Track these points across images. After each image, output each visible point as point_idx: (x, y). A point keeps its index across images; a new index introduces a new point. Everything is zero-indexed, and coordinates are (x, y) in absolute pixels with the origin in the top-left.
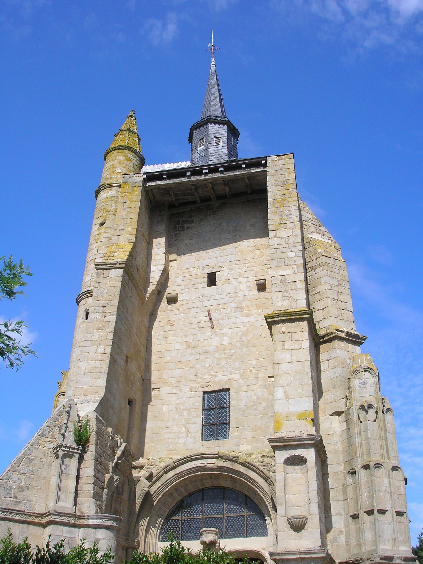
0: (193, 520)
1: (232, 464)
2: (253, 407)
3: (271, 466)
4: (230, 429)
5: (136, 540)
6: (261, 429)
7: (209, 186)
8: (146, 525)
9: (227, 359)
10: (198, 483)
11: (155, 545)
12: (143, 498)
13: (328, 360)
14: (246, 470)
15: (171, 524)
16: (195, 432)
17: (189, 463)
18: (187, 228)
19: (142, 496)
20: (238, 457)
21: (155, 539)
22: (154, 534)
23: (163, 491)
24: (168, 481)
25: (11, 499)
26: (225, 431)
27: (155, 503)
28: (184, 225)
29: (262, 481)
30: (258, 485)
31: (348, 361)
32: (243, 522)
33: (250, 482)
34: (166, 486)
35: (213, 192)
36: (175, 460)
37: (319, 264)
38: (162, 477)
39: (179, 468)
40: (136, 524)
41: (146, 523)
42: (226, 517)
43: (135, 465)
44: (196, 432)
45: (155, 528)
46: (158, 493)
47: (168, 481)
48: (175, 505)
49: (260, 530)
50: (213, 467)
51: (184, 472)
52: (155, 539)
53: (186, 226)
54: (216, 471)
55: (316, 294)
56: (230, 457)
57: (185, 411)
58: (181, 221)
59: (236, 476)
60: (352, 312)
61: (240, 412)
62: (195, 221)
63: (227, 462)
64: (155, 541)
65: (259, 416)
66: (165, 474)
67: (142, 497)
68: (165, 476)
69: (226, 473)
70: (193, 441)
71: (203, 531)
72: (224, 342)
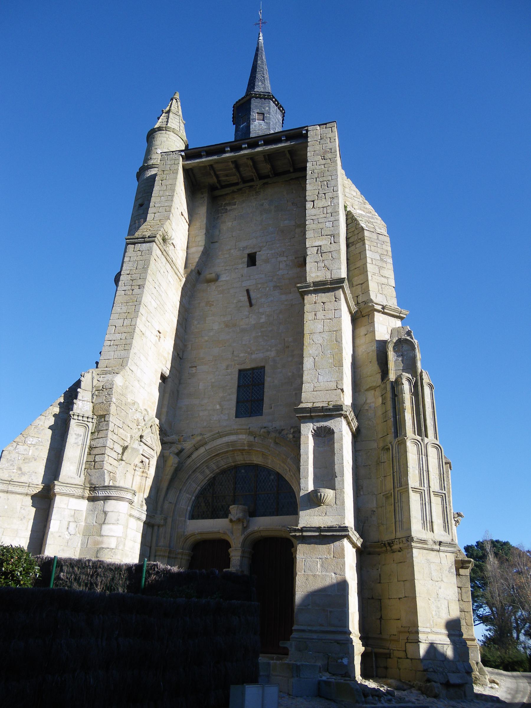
7: (250, 164)
9: (264, 337)
13: (365, 335)
18: (229, 210)
21: (396, 481)
25: (15, 470)
28: (226, 208)
31: (387, 335)
35: (254, 171)
37: (360, 239)
53: (228, 208)
55: (356, 269)
58: (223, 204)
60: (394, 287)
62: (237, 203)
72: (262, 320)
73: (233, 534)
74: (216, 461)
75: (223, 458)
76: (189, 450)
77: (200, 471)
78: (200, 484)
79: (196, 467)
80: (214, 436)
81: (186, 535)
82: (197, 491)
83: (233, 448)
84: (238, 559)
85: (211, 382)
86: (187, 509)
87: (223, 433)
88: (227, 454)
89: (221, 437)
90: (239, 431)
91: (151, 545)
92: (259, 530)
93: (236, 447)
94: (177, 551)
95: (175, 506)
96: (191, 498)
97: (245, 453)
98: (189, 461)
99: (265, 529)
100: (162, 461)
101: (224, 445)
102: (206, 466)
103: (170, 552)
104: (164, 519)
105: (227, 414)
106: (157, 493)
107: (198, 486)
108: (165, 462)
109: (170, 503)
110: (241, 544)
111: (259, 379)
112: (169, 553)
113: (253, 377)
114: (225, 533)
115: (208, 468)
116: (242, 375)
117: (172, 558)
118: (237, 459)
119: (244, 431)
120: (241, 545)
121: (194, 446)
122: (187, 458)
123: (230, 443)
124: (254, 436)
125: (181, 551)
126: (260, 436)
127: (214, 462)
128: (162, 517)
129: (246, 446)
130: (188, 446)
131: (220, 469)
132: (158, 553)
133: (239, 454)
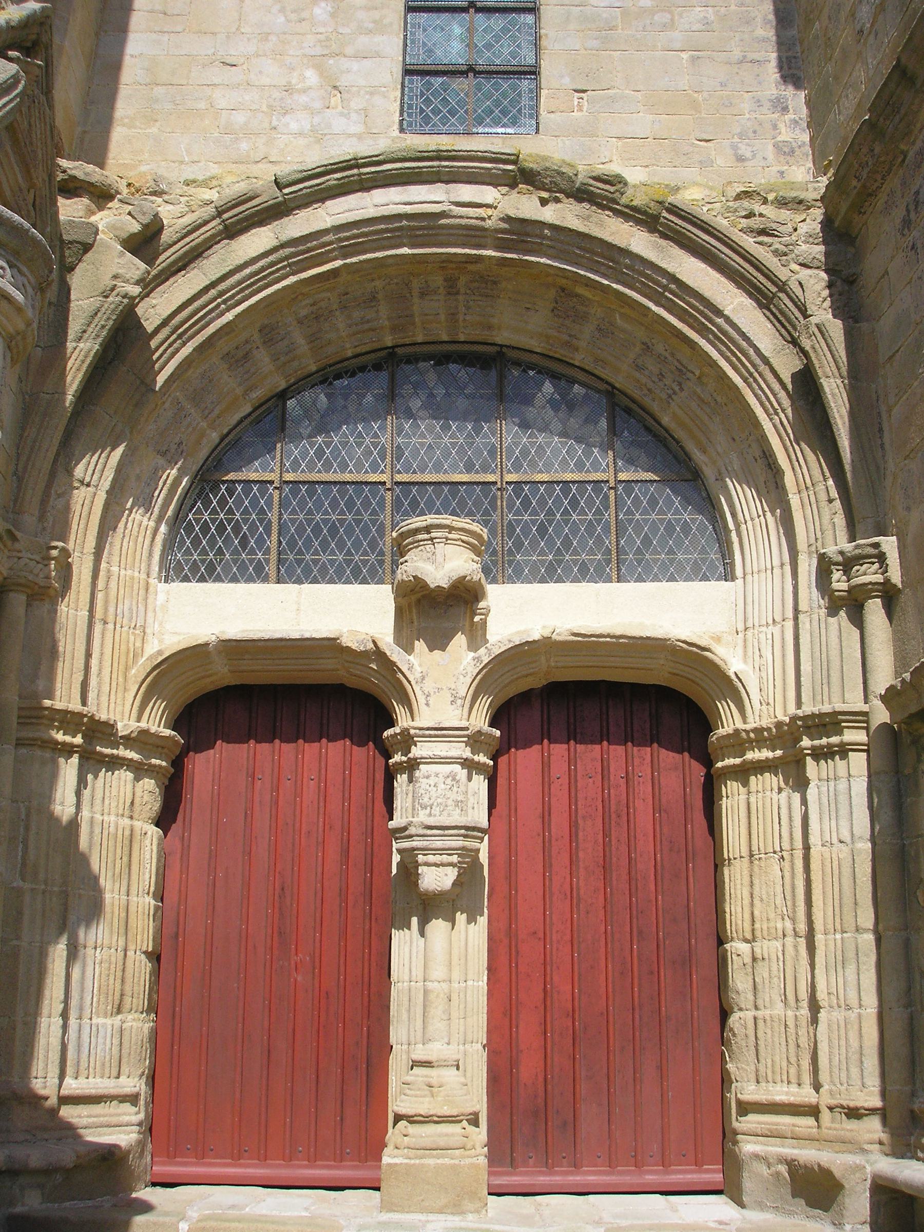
1: (589, 217)
2: (656, 18)
3: (794, 238)
4: (544, 93)
5: (55, 548)
6: (695, 106)
8: (106, 484)
10: (384, 310)
11: (142, 592)
12: (105, 333)
14: (660, 249)
15: (223, 502)
16: (367, 93)
17: (359, 194)
19: (105, 322)
20: (616, 181)
21: (143, 565)
22: (140, 539)
23: (208, 324)
24: (238, 277)
27: (161, 380)
29: (741, 304)
30: (720, 321)
32: (598, 512)
33: (671, 308)
34: (224, 302)
36: (285, 170)
38: (210, 252)
39: (303, 214)
40: (53, 474)
41: (109, 475)
42: (511, 483)
44: (372, 94)
45: (148, 508)
46: (181, 330)
47: (238, 277)
48: (249, 414)
50: (483, 223)
51: (326, 239)
52: (143, 565)
54: (497, 248)
56: (581, 178)
57: (323, 4)
59: (597, 278)
61: (590, 30)
63: (559, 205)
64: (143, 576)
65: (685, 55)
66: (226, 241)
67: (103, 327)
68: (222, 251)
69: (549, 262)
70: (358, 129)
71: (417, 531)
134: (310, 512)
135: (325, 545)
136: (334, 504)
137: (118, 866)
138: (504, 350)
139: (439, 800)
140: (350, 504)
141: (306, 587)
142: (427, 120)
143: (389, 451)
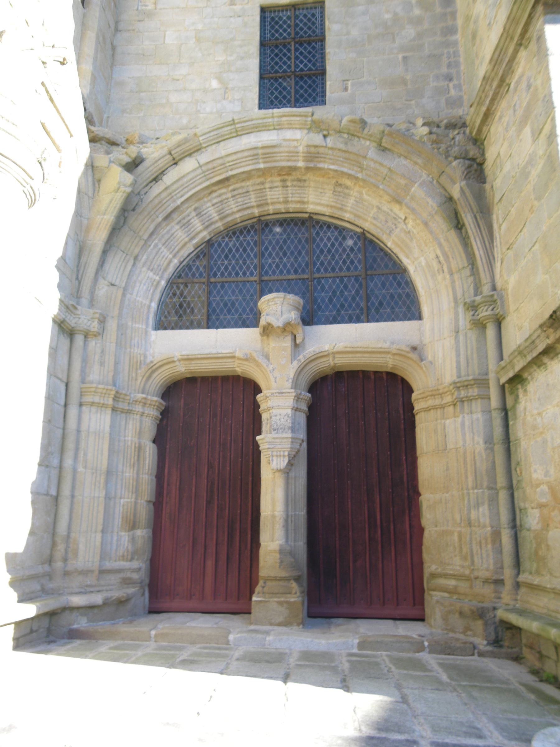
0: (237, 286)
26: (314, 90)
43: (97, 133)
49: (400, 308)
73: (268, 359)
74: (220, 199)
75: (235, 193)
76: (157, 161)
77: (180, 221)
78: (178, 252)
79: (173, 206)
80: (220, 131)
81: (152, 362)
82: (171, 269)
83: (268, 165)
84: (287, 415)
85: (195, 30)
86: (149, 307)
87: (245, 124)
88: (248, 184)
89: (237, 136)
90: (284, 119)
91: (68, 376)
92: (335, 350)
93: (275, 161)
94: (132, 395)
95: (124, 295)
96: (159, 282)
97: (293, 180)
98: (157, 189)
99: (348, 349)
100: (90, 179)
101: (246, 154)
102: (195, 209)
103: (116, 398)
104: (99, 320)
105: (238, 100)
106: (80, 257)
107: (174, 256)
108: (97, 185)
109: (112, 285)
110: (291, 381)
111: (309, 28)
112: (114, 399)
113: (297, 25)
114: (248, 359)
115: (199, 215)
116: (269, 19)
117: (122, 412)
118: (269, 197)
119: (298, 119)
120: (292, 382)
121: (170, 153)
122: (151, 182)
123: (260, 151)
124: (325, 133)
125: (140, 396)
126: (340, 132)
127: (215, 201)
128: (95, 313)
129: (301, 158)
130: (153, 153)
131: (210, 229)
132: (88, 399)
133: (276, 184)
134: (222, 296)
135: (229, 311)
136: (233, 292)
137: (132, 460)
138: (312, 215)
139: (281, 427)
140: (241, 291)
141: (220, 330)
142: (272, 102)
143: (258, 266)
